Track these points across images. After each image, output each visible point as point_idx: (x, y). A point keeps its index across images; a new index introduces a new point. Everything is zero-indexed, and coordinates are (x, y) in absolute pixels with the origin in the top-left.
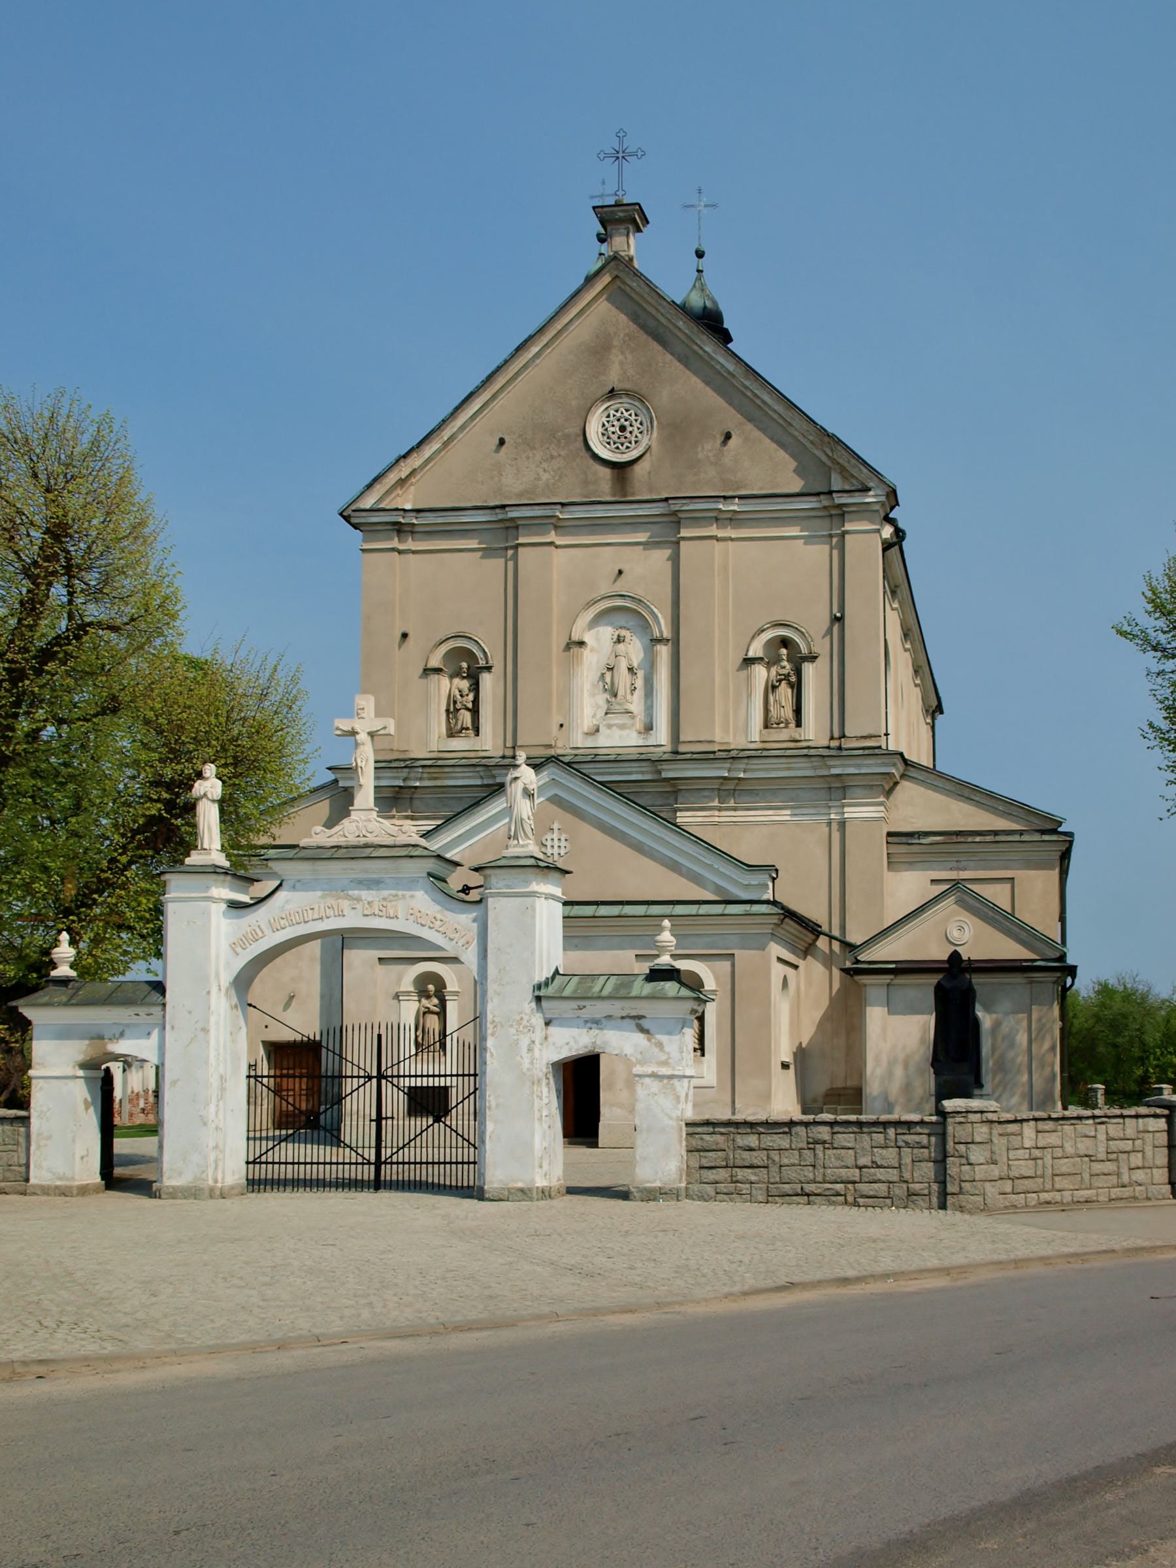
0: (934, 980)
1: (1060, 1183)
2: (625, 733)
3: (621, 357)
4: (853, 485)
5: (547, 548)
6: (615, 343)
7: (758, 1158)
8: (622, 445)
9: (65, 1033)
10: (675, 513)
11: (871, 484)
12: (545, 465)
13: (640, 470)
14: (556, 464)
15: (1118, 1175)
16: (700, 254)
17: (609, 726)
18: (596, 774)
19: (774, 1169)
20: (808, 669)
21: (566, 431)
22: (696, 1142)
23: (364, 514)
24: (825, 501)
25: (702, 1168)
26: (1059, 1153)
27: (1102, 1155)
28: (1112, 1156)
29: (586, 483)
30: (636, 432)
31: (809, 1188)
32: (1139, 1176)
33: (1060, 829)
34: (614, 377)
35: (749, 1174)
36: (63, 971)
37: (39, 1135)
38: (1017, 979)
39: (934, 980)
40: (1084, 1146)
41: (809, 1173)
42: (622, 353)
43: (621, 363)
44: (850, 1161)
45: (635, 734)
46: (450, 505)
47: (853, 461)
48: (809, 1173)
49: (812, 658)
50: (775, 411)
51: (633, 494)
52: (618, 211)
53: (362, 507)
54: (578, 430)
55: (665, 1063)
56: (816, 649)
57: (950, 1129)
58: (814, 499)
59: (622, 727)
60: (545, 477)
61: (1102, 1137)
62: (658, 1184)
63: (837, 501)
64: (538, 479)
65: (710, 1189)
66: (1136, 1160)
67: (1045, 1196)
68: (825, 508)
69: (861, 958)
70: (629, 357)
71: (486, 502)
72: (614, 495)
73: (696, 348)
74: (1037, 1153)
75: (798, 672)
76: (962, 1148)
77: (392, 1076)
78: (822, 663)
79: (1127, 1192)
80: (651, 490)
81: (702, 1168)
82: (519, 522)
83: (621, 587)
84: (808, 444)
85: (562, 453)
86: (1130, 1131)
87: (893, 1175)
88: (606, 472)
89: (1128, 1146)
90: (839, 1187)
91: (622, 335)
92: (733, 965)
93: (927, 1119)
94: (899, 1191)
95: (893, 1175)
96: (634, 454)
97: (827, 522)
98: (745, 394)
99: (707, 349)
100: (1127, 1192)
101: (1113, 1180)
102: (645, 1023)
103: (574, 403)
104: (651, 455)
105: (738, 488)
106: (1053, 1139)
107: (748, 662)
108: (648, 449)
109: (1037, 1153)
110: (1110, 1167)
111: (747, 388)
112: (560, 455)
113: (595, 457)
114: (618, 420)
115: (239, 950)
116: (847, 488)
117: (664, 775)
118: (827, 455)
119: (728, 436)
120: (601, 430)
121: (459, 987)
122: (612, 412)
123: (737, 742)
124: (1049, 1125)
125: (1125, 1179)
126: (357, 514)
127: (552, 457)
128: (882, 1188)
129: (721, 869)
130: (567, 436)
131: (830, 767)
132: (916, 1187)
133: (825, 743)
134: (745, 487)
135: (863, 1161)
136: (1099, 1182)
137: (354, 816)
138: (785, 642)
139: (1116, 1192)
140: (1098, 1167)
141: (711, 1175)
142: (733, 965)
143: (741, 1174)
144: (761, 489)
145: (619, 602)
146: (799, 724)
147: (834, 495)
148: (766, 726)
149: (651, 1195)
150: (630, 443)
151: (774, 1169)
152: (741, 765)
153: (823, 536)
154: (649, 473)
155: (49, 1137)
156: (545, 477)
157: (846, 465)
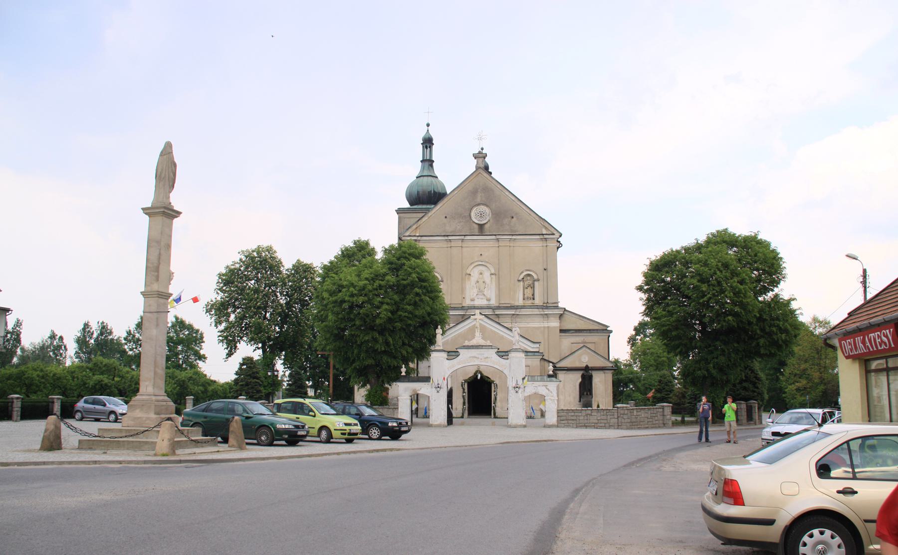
0: (581, 373)
1: (641, 423)
2: (483, 300)
3: (481, 194)
6: (479, 190)
7: (573, 418)
9: (406, 390)
10: (498, 239)
13: (487, 226)
14: (462, 224)
15: (653, 422)
16: (428, 125)
17: (478, 298)
18: (502, 323)
19: (578, 420)
20: (536, 283)
22: (745, 421)
25: (561, 420)
26: (641, 416)
27: (649, 417)
28: (652, 417)
29: (470, 229)
31: (586, 425)
32: (657, 422)
33: (608, 329)
34: (478, 200)
35: (573, 422)
36: (403, 374)
37: (401, 412)
38: (601, 372)
39: (581, 373)
40: (646, 415)
41: (586, 421)
43: (481, 196)
44: (596, 418)
45: (486, 301)
47: (549, 226)
48: (586, 421)
49: (538, 280)
53: (405, 235)
54: (468, 214)
55: (552, 396)
56: (448, 333)
57: (619, 411)
59: (482, 299)
60: (458, 227)
61: (649, 413)
62: (551, 424)
65: (563, 425)
66: (656, 418)
67: (639, 426)
69: (557, 366)
70: (483, 195)
74: (637, 417)
75: (534, 284)
76: (622, 415)
78: (541, 282)
79: (654, 426)
80: (490, 232)
81: (561, 420)
83: (481, 258)
86: (655, 412)
87: (605, 421)
89: (654, 415)
90: (593, 424)
93: (578, 409)
94: (607, 425)
95: (605, 421)
96: (485, 222)
97: (541, 242)
100: (654, 426)
101: (652, 423)
102: (548, 387)
103: (467, 207)
105: (515, 232)
106: (639, 413)
107: (519, 281)
108: (489, 220)
109: (637, 417)
110: (651, 420)
113: (474, 222)
115: (449, 369)
116: (548, 233)
117: (496, 313)
118: (541, 224)
119: (513, 217)
120: (475, 215)
123: (517, 304)
124: (639, 410)
125: (654, 423)
127: (461, 222)
128: (603, 425)
130: (465, 216)
131: (544, 312)
132: (611, 424)
133: (542, 304)
134: (518, 232)
135: (599, 418)
136: (649, 423)
137: (476, 338)
138: (529, 275)
139: (652, 426)
140: (649, 420)
141: (563, 422)
143: (570, 422)
145: (481, 263)
146: (534, 299)
148: (524, 299)
149: (515, 427)
151: (578, 420)
152: (518, 310)
155: (403, 413)
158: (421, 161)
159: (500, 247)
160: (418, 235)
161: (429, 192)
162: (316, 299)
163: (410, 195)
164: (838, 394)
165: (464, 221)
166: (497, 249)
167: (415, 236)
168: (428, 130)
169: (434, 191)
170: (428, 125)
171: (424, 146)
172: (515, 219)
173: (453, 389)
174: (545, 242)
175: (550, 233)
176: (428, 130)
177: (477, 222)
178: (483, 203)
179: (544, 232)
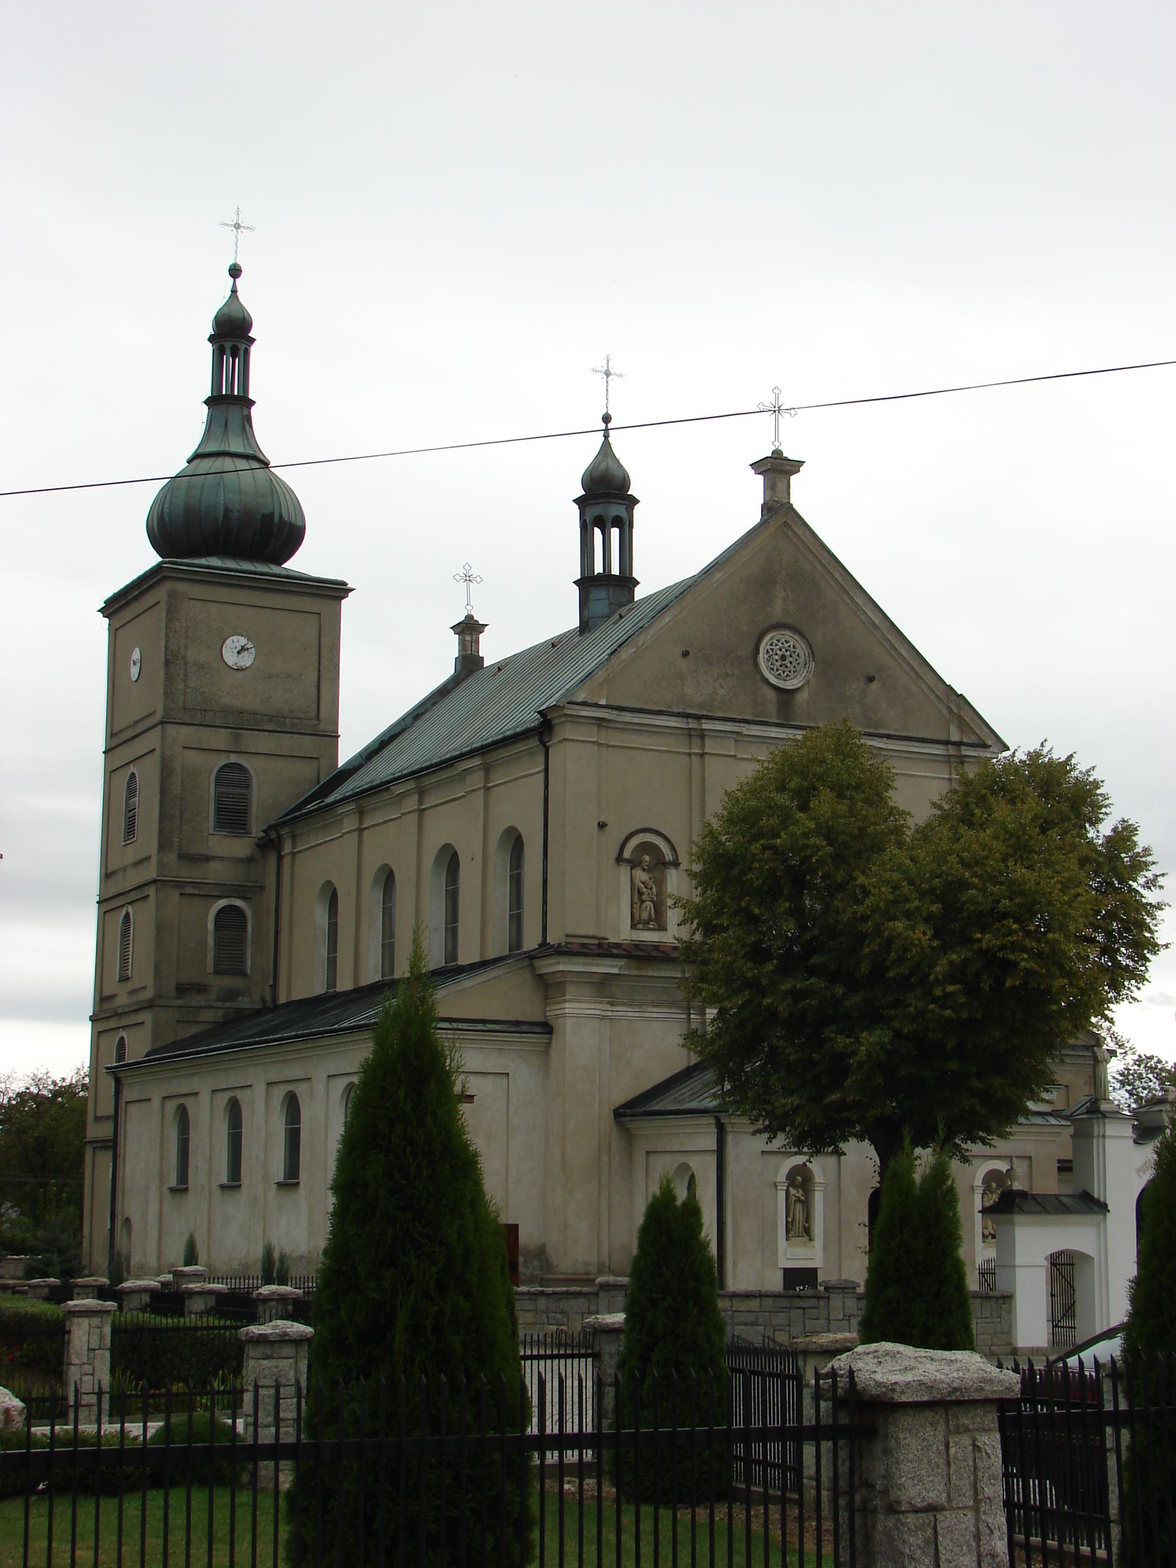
4: (970, 739)
5: (729, 759)
8: (784, 672)
11: (989, 743)
12: (721, 681)
16: (235, 272)
21: (739, 653)
23: (577, 707)
24: (952, 751)
30: (794, 663)
42: (785, 590)
46: (638, 706)
50: (909, 664)
51: (795, 720)
52: (787, 465)
53: (574, 699)
58: (942, 747)
60: (721, 692)
63: (964, 753)
64: (715, 693)
68: (949, 756)
71: (670, 707)
72: (779, 719)
73: (845, 597)
77: (1059, 1264)
82: (706, 733)
84: (933, 698)
85: (736, 672)
88: (771, 694)
91: (785, 573)
92: (1030, 1166)
98: (882, 645)
99: (857, 601)
104: (809, 687)
111: (887, 639)
112: (733, 675)
113: (767, 682)
114: (780, 650)
118: (949, 708)
119: (871, 679)
121: (824, 1179)
122: (775, 642)
126: (571, 706)
127: (727, 675)
129: (289, 1057)
142: (1030, 1166)
144: (896, 730)
147: (963, 748)
150: (790, 672)
153: (943, 778)
154: (808, 702)
156: (721, 692)
157: (970, 723)
158: (208, 402)
159: (707, 758)
160: (603, 702)
161: (264, 517)
162: (1015, 964)
163: (161, 517)
164: (798, 1165)
165: (736, 672)
166: (686, 758)
167: (597, 705)
168: (234, 291)
169: (281, 516)
170: (235, 272)
171: (228, 346)
172: (874, 686)
173: (196, 1235)
174: (696, 742)
175: (974, 740)
176: (234, 291)
177: (773, 680)
178: (789, 621)
179: (955, 737)
